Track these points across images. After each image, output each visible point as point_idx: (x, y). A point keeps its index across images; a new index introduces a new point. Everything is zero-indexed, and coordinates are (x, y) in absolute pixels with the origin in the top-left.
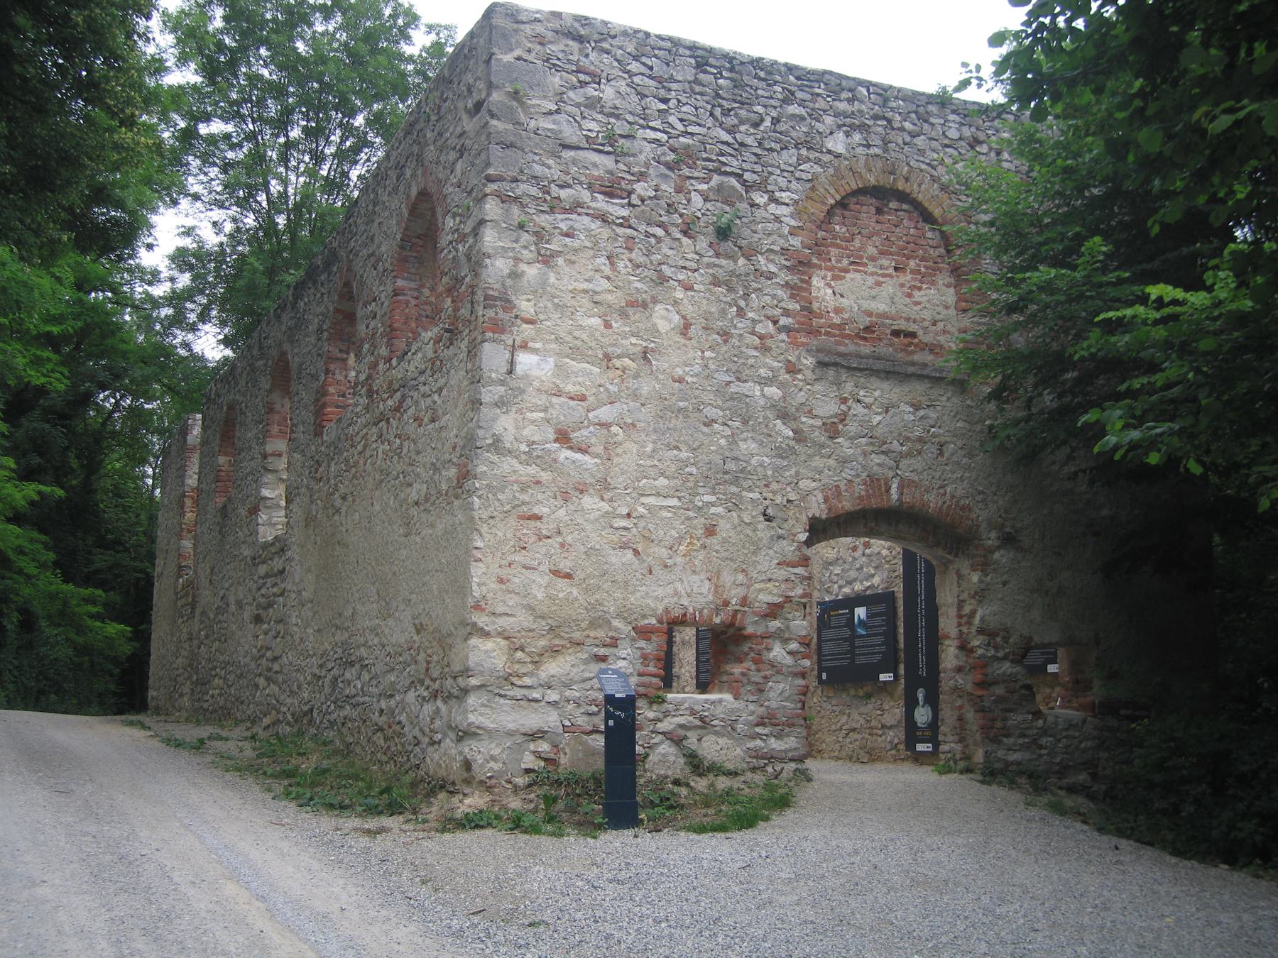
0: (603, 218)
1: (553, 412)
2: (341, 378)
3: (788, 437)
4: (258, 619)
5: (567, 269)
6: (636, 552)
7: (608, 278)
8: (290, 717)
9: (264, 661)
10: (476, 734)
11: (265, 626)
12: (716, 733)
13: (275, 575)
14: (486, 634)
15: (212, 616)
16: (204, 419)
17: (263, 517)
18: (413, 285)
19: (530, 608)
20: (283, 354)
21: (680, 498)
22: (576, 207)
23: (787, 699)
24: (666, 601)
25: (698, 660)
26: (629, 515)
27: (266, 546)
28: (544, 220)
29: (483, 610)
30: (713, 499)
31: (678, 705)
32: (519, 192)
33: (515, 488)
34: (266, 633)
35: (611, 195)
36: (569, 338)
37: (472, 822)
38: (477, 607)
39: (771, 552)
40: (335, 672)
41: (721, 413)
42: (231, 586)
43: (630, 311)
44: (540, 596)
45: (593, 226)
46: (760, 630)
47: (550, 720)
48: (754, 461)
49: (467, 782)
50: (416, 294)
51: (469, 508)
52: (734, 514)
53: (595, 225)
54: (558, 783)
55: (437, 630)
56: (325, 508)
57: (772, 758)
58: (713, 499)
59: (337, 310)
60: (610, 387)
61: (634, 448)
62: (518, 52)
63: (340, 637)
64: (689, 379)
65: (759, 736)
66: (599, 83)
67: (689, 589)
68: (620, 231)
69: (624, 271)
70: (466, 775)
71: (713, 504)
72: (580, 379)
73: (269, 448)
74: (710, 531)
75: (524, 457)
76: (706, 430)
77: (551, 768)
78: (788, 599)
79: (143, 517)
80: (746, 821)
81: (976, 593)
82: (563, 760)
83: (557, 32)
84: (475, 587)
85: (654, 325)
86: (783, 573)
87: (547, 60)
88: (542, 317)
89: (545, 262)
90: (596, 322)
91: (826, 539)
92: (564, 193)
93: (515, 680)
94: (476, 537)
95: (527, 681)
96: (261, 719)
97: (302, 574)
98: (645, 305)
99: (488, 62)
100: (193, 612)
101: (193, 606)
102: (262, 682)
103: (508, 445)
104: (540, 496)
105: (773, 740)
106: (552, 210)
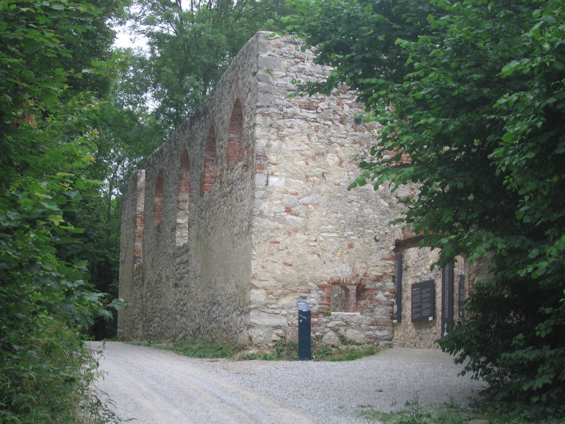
0: (305, 119)
1: (284, 201)
2: (212, 169)
3: (386, 206)
4: (176, 285)
5: (290, 142)
6: (319, 255)
7: (307, 144)
8: (191, 332)
9: (179, 307)
10: (253, 326)
11: (180, 289)
12: (353, 328)
13: (184, 263)
14: (257, 288)
15: (153, 285)
16: (146, 173)
17: (178, 233)
18: (237, 136)
19: (275, 278)
20: (186, 151)
21: (337, 233)
22: (294, 115)
23: (384, 315)
24: (331, 275)
25: (412, 308)
26: (316, 241)
27: (179, 248)
28: (280, 122)
29: (256, 279)
30: (352, 233)
31: (336, 316)
32: (270, 112)
33: (269, 231)
34: (180, 292)
35: (309, 109)
36: (291, 170)
37: (251, 358)
38: (254, 278)
39: (378, 255)
40: (209, 308)
41: (356, 197)
42: (163, 268)
43: (317, 157)
44: (279, 273)
45: (301, 123)
46: (372, 287)
47: (283, 321)
48: (370, 217)
49: (251, 345)
50: (238, 140)
51: (251, 239)
52: (361, 239)
53: (302, 123)
54: (285, 345)
55: (242, 287)
56: (205, 232)
57: (377, 338)
58: (352, 233)
59: (209, 137)
60: (308, 189)
61: (318, 213)
62: (269, 53)
63: (211, 292)
64: (342, 184)
65: (371, 330)
66: (304, 62)
67: (341, 270)
68: (313, 124)
69: (314, 141)
70: (250, 342)
71: (352, 235)
72: (295, 186)
73: (180, 198)
74: (351, 246)
75: (272, 219)
76: (349, 205)
77: (283, 340)
78: (385, 274)
79: (102, 216)
80: (352, 358)
81: (475, 271)
82: (288, 337)
83: (285, 42)
84: (253, 270)
85: (327, 162)
86: (383, 263)
87: (282, 55)
88: (279, 162)
89: (281, 140)
90: (302, 163)
91: (414, 247)
92: (289, 110)
93: (269, 306)
94: (253, 250)
95: (274, 306)
96: (178, 335)
97: (195, 264)
98: (323, 154)
99: (258, 56)
100: (143, 283)
101: (143, 279)
102: (178, 317)
103: (266, 214)
104: (279, 234)
105: (377, 331)
106: (284, 118)
